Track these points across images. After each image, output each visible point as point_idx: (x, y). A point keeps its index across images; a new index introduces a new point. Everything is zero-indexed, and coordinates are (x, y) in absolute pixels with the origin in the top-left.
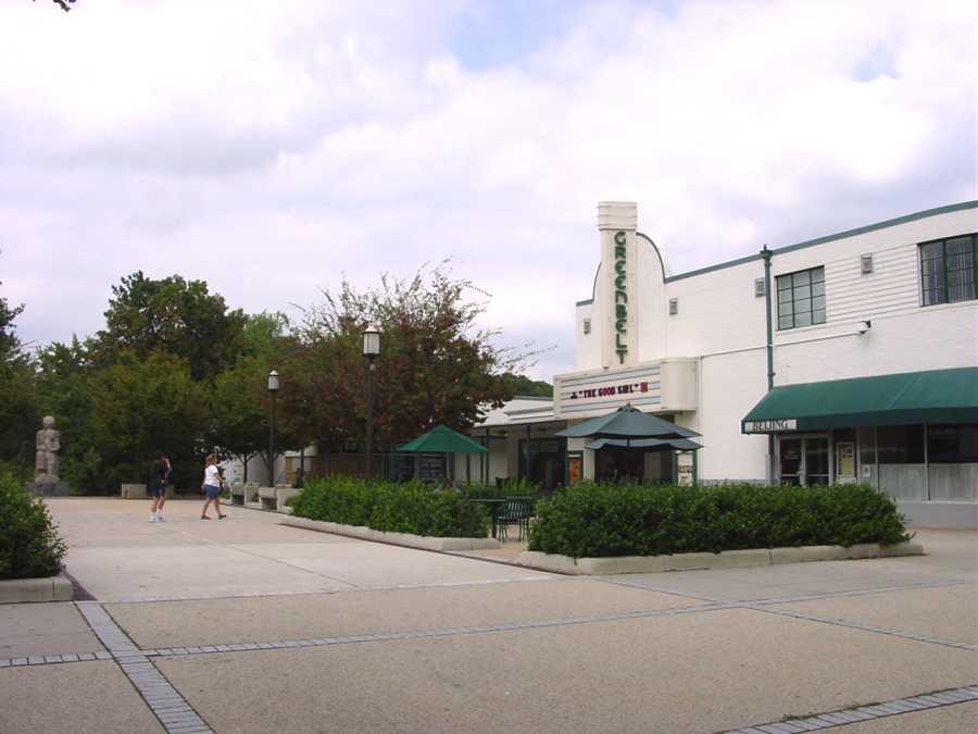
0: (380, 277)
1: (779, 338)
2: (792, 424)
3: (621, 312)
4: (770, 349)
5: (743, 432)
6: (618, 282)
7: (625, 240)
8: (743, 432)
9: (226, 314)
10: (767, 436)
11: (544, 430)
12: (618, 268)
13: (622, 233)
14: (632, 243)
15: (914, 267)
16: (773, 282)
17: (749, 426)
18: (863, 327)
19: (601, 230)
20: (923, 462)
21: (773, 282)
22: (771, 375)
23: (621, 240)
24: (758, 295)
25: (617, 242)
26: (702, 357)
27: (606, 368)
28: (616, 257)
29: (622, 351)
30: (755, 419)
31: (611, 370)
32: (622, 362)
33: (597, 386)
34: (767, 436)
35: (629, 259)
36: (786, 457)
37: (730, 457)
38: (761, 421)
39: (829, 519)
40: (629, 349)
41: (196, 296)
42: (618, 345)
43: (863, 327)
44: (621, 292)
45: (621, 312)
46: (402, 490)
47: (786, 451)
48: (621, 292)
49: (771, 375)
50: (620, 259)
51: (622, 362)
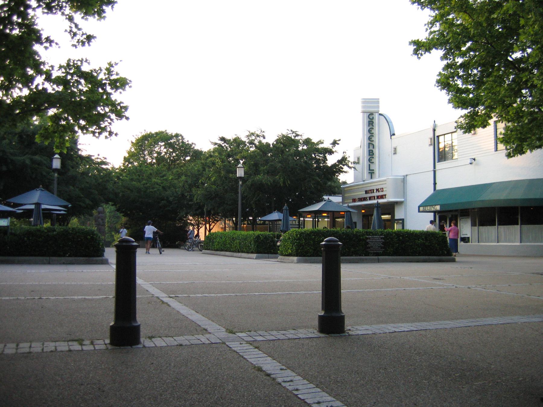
1: (439, 165)
2: (438, 208)
4: (435, 172)
5: (419, 211)
6: (370, 138)
8: (419, 211)
9: (415, 47)
10: (432, 214)
12: (370, 131)
17: (421, 209)
20: (518, 224)
22: (435, 184)
23: (371, 117)
24: (431, 145)
26: (407, 175)
29: (371, 173)
32: (371, 178)
34: (432, 214)
37: (420, 222)
38: (426, 206)
42: (370, 170)
49: (435, 184)
50: (371, 127)
51: (371, 178)
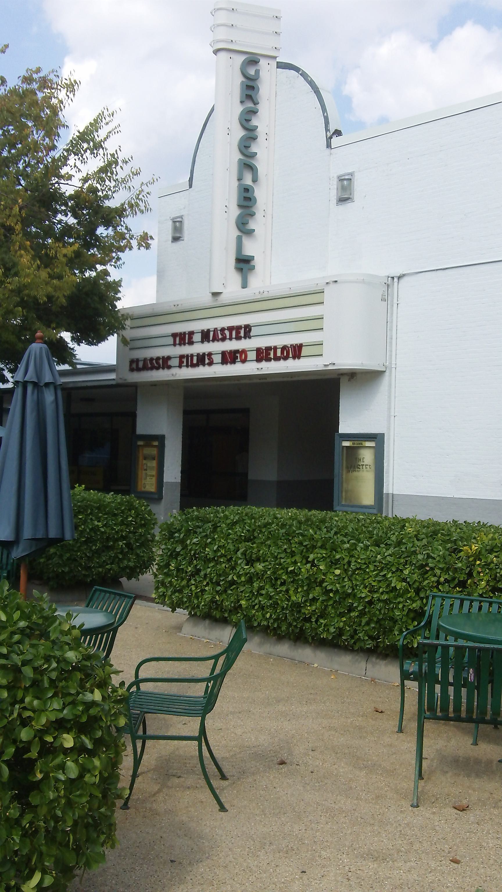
0: (375, 712)
3: (247, 200)
7: (257, 72)
13: (252, 60)
14: (268, 75)
15: (105, 595)
19: (216, 52)
23: (252, 72)
25: (244, 75)
27: (216, 294)
28: (242, 102)
29: (244, 263)
31: (224, 299)
32: (244, 285)
33: (198, 326)
35: (263, 108)
39: (283, 526)
40: (258, 262)
41: (421, 562)
44: (248, 164)
45: (247, 200)
48: (248, 164)
51: (244, 285)
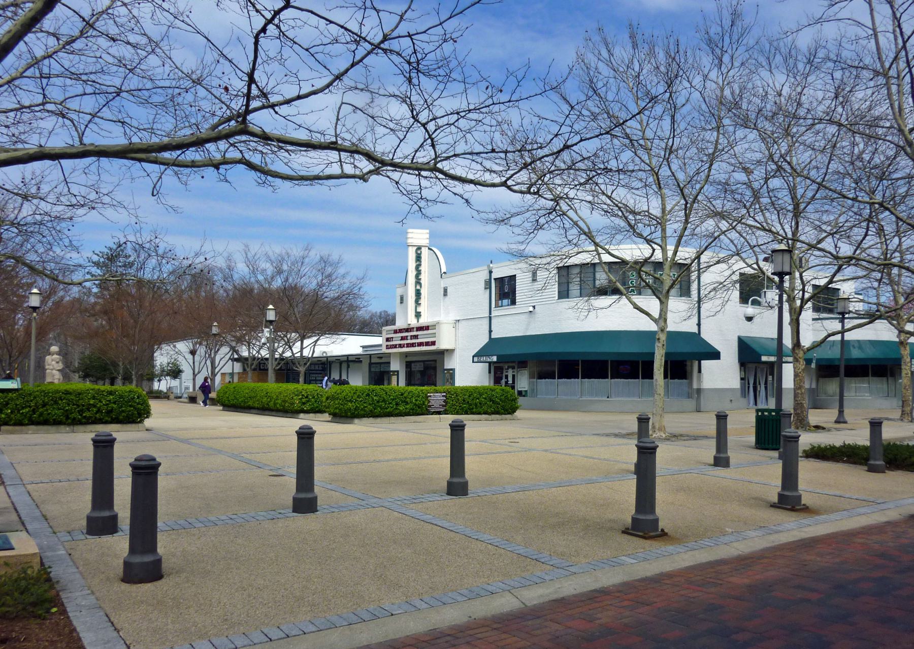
2: (495, 359)
4: (490, 318)
11: (381, 358)
16: (493, 281)
17: (476, 359)
18: (531, 309)
21: (493, 281)
22: (490, 331)
30: (479, 355)
36: (373, 370)
42: (416, 312)
43: (531, 309)
46: (97, 387)
47: (497, 372)
49: (490, 331)
